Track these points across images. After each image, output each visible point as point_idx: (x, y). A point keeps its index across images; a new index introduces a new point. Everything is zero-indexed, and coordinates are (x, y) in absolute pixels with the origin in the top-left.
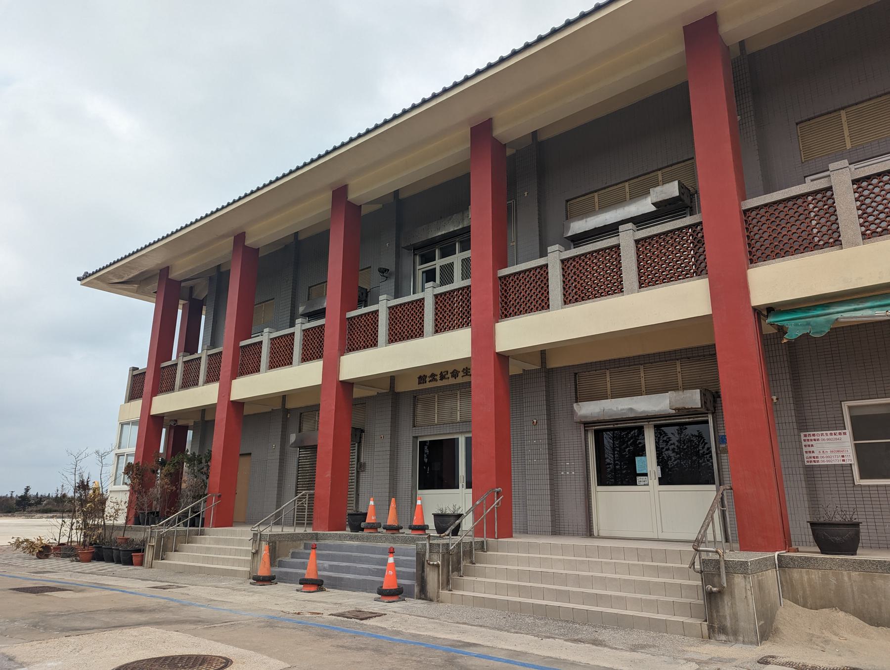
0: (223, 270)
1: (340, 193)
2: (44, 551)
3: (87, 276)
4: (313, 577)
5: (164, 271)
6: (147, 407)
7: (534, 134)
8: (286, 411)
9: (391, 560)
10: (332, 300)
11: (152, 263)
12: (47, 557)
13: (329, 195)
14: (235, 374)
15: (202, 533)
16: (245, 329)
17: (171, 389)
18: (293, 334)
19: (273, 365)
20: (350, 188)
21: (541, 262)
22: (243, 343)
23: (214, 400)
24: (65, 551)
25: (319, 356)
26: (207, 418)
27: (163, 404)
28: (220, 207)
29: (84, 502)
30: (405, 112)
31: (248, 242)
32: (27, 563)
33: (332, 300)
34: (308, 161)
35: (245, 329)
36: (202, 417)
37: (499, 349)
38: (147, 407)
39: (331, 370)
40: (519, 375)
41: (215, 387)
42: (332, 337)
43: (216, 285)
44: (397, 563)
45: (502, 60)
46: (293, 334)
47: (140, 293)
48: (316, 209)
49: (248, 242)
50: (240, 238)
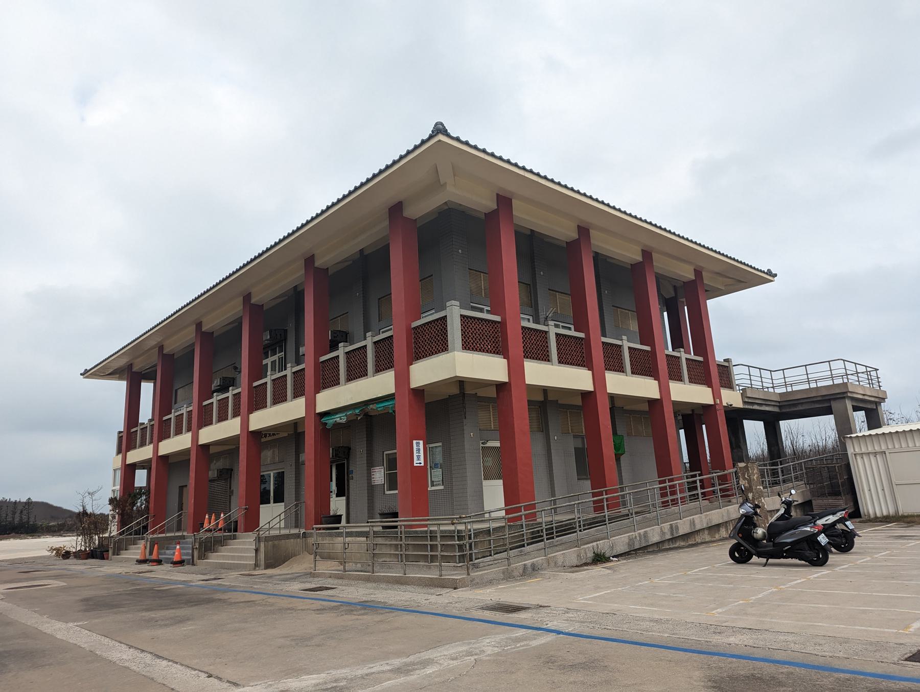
0: (299, 289)
1: (309, 261)
2: (67, 555)
3: (86, 371)
4: (179, 559)
5: (130, 366)
6: (124, 459)
7: (361, 251)
8: (367, 416)
9: (178, 547)
10: (308, 349)
11: (123, 362)
12: (68, 558)
13: (302, 263)
14: (319, 388)
15: (235, 538)
16: (258, 372)
17: (336, 382)
18: (366, 346)
19: (350, 378)
20: (253, 295)
21: (441, 314)
22: (255, 384)
23: (189, 446)
24: (80, 555)
25: (239, 415)
26: (299, 431)
27: (134, 456)
28: (364, 180)
29: (84, 522)
30: (402, 157)
31: (317, 264)
32: (58, 562)
33: (308, 349)
34: (418, 142)
35: (206, 393)
36: (229, 446)
37: (414, 385)
38: (124, 459)
39: (403, 378)
40: (451, 397)
41: (302, 401)
42: (400, 349)
43: (181, 362)
44: (180, 549)
45: (423, 142)
46: (366, 346)
47: (120, 379)
48: (295, 275)
49: (317, 264)
50: (247, 298)
